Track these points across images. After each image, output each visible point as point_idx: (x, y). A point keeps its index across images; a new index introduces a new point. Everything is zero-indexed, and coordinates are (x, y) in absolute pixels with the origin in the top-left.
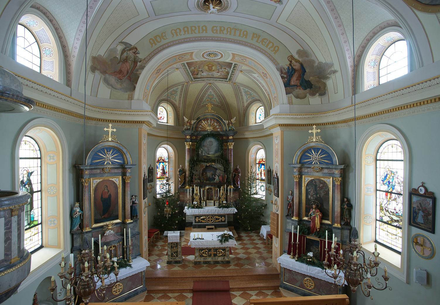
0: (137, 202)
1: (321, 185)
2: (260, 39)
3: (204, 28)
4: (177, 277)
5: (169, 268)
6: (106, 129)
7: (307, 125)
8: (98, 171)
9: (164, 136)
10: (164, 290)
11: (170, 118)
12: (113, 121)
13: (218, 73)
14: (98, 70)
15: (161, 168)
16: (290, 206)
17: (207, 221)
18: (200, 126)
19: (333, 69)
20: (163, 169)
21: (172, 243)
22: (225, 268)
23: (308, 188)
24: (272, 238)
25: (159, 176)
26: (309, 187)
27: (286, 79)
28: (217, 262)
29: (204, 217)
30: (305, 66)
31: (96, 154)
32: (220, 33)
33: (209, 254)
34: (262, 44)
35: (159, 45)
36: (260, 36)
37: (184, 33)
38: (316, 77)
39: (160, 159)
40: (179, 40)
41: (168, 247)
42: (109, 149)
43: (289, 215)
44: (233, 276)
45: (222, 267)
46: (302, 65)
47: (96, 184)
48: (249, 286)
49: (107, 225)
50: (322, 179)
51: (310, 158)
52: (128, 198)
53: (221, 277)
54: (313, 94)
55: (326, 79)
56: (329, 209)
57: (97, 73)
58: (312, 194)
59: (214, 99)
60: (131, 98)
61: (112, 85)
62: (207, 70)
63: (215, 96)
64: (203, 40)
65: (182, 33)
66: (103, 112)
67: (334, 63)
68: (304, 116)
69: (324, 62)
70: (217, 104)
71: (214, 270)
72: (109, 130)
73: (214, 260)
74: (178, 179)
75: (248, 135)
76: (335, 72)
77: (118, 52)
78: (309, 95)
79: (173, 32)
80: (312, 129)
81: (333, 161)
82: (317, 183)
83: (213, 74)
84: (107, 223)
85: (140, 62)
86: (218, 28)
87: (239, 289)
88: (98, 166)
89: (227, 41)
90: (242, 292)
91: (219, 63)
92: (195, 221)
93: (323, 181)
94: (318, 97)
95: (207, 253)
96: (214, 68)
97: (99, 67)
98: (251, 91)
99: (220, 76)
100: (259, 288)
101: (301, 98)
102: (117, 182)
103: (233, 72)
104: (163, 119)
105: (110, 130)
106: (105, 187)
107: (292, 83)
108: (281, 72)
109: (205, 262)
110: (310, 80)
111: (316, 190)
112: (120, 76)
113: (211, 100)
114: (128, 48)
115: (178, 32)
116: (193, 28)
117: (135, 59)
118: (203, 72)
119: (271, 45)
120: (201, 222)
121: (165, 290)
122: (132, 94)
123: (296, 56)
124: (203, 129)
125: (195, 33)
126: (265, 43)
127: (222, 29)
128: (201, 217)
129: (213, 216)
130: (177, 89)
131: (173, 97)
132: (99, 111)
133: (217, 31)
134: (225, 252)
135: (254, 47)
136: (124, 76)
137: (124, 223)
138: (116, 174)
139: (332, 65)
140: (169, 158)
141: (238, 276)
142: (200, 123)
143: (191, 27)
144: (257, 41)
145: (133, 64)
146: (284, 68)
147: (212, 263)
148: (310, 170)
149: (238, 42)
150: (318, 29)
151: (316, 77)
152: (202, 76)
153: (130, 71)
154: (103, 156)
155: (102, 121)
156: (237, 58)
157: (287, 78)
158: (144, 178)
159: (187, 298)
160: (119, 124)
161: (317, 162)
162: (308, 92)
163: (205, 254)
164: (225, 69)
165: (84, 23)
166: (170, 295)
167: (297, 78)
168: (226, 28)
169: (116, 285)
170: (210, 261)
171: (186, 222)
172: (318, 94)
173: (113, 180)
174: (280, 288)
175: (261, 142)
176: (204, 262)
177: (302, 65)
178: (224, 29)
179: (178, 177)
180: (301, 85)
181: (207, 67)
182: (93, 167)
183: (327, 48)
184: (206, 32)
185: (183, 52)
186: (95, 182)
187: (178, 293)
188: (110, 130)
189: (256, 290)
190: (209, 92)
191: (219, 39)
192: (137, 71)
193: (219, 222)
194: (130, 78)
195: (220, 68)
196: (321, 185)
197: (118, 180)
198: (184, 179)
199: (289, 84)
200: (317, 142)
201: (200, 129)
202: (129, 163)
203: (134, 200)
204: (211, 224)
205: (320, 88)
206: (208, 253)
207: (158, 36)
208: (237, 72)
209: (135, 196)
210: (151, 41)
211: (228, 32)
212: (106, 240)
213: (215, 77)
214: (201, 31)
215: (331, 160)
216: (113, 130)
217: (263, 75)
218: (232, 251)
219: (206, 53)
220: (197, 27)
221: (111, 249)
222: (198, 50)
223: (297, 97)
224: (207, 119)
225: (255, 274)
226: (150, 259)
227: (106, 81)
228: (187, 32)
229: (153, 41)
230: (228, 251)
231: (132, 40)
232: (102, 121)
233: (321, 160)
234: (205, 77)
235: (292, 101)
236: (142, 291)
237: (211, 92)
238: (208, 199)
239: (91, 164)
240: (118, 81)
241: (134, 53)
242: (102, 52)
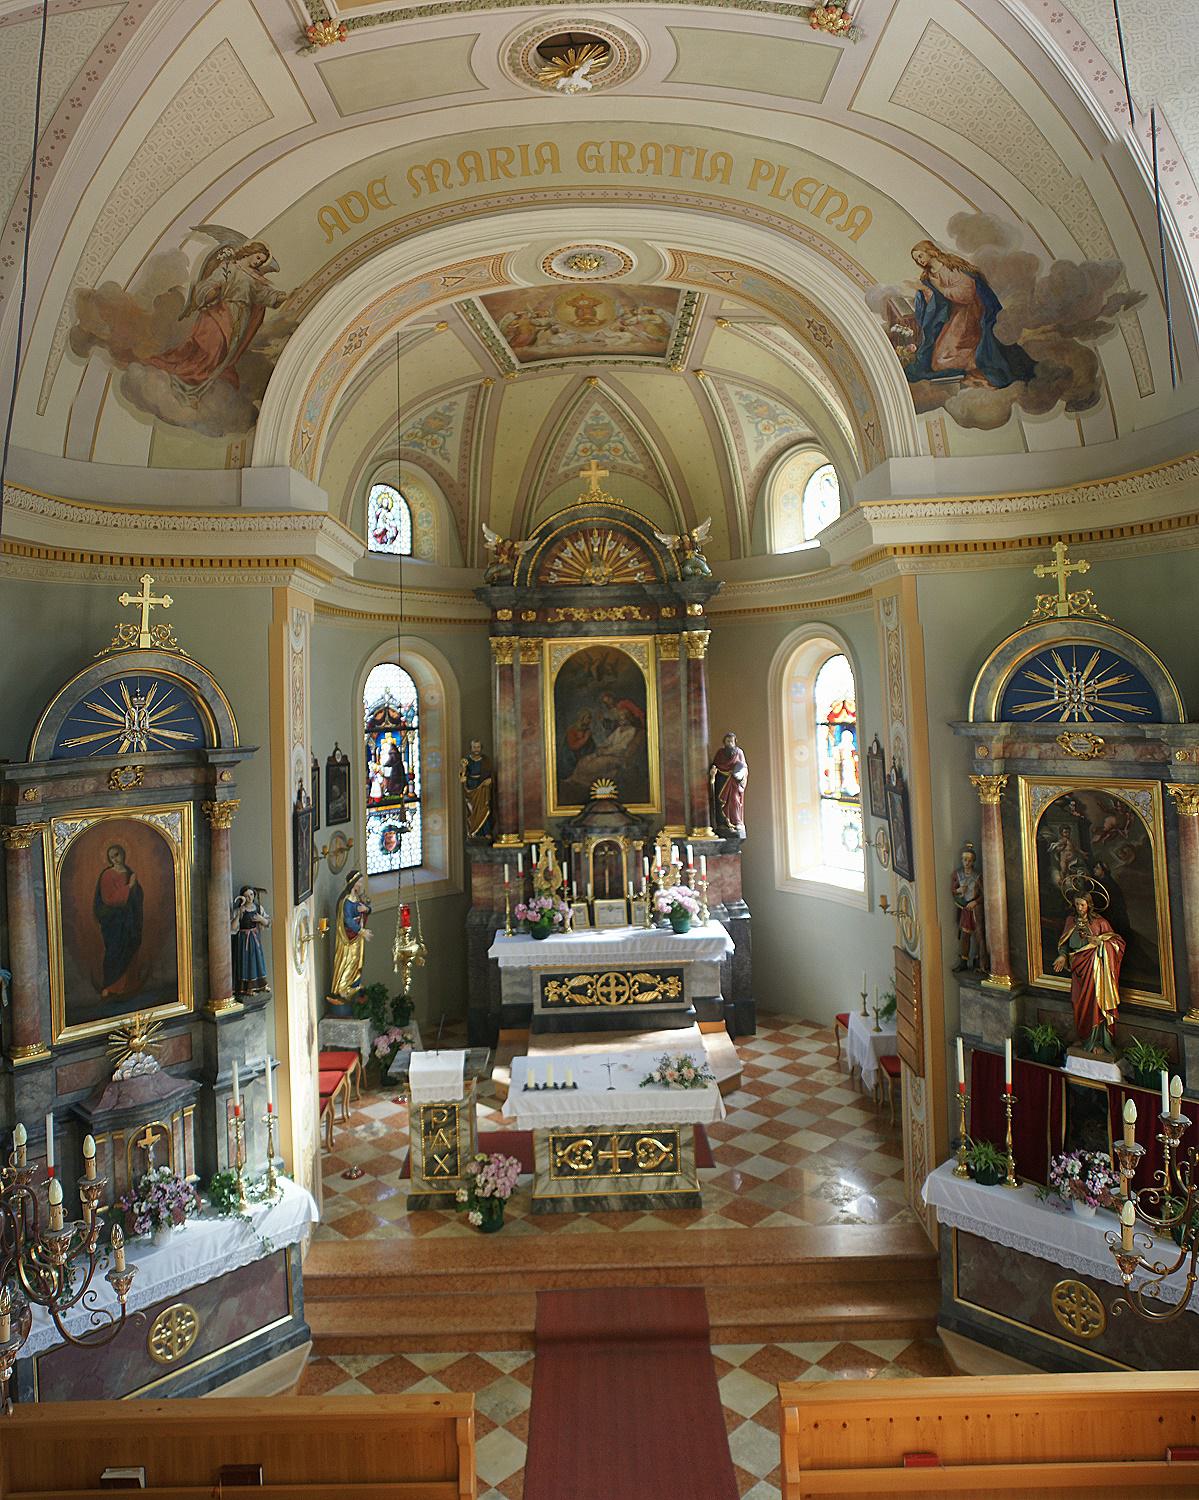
0: (263, 917)
1: (1110, 821)
2: (788, 183)
3: (546, 153)
4: (452, 1271)
5: (418, 1230)
6: (126, 599)
7: (1004, 543)
8: (90, 785)
9: (388, 612)
10: (391, 1337)
11: (425, 534)
12: (132, 560)
13: (622, 330)
14: (102, 343)
15: (385, 757)
16: (968, 918)
17: (598, 1000)
18: (558, 565)
19: (1122, 289)
20: (396, 761)
21: (427, 1109)
22: (677, 1223)
23: (1046, 835)
24: (896, 1075)
25: (376, 792)
26: (1051, 830)
27: (913, 347)
28: (636, 1204)
29: (585, 980)
30: (993, 282)
31: (81, 710)
32: (614, 169)
33: (601, 1163)
34: (799, 204)
35: (357, 232)
36: (783, 171)
37: (462, 179)
38: (1049, 327)
39: (380, 717)
40: (442, 206)
41: (412, 1126)
42: (140, 684)
43: (971, 965)
44: (713, 1267)
45: (666, 1219)
46: (979, 280)
47: (68, 841)
48: (789, 1320)
49: (127, 1033)
50: (1112, 791)
51: (106, 724)
52: (224, 899)
53: (658, 1269)
54: (1040, 405)
55: (1097, 335)
56: (1157, 939)
57: (99, 359)
58: (1067, 863)
59: (613, 445)
60: (240, 461)
61: (157, 408)
62: (572, 323)
63: (617, 429)
64: (566, 200)
65: (456, 176)
66: (116, 526)
67: (694, 1121)
68: (1002, 507)
69: (1078, 260)
70: (629, 463)
71: (625, 1233)
72: (139, 600)
73: (625, 1192)
74: (465, 806)
75: (763, 593)
76: (1132, 300)
77: (189, 269)
78: (1024, 407)
79: (418, 174)
80: (1049, 559)
81: (1157, 702)
82: (1087, 812)
83: (598, 338)
84: (127, 1021)
85: (275, 306)
86: (606, 150)
87: (743, 1334)
88: (90, 760)
89: (644, 201)
90: (759, 1347)
91: (620, 292)
92: (544, 998)
93: (1118, 800)
94: (1062, 415)
95: (589, 1155)
96: (600, 312)
97: (107, 330)
98: (772, 403)
99: (633, 345)
100: (841, 1329)
101: (986, 426)
102: (173, 828)
103: (686, 325)
104: (394, 539)
105: (147, 601)
106: (112, 852)
107: (942, 360)
108: (892, 318)
109: (586, 1200)
110: (1020, 343)
111: (1084, 843)
112: (193, 367)
113: (600, 450)
114: (230, 248)
115: (437, 176)
116: (502, 156)
117: (253, 294)
118: (556, 332)
119: (834, 203)
120: (573, 1004)
121: (398, 1336)
122: (244, 443)
123: (949, 244)
124: (570, 576)
125: (509, 175)
126: (810, 196)
127: (623, 150)
128: (571, 977)
129: (624, 974)
130: (449, 408)
131: (435, 442)
132: (98, 523)
133: (599, 160)
134: (673, 1151)
135: (762, 216)
136: (210, 369)
137: (203, 1015)
138: (168, 796)
139: (1116, 271)
140: (422, 708)
141: (736, 1265)
142: (554, 551)
143: (493, 152)
144: (774, 193)
145: (246, 315)
146: (901, 300)
147: (615, 1205)
148: (1052, 749)
149: (692, 201)
150: (1029, 123)
151: (1049, 327)
152: (555, 350)
153: (232, 347)
154: (114, 716)
155: (112, 563)
156: (691, 268)
157: (915, 339)
158: (296, 807)
159: (496, 1373)
160: (188, 571)
161: (1080, 714)
162: (1015, 395)
163: (584, 1161)
164: (651, 312)
165: (19, 227)
166: (419, 1360)
167: (963, 337)
168: (638, 148)
169: (169, 1317)
170: (606, 1197)
171: (504, 1002)
172: (1061, 403)
173: (157, 820)
174: (939, 1329)
175: (837, 628)
176: (575, 1200)
177: (979, 280)
178: (631, 154)
179: (465, 795)
180: (981, 365)
181: (571, 310)
182: (64, 769)
183: (1088, 198)
184: (556, 169)
185: (503, 245)
186: (64, 831)
187: (455, 1350)
188: (147, 601)
189: (825, 1339)
190: (589, 415)
191: (611, 194)
192: (264, 343)
193: (654, 1001)
194: (233, 378)
195: (628, 309)
196: (1110, 821)
197: (177, 824)
198: (491, 802)
199: (930, 361)
200: (1075, 617)
201: (554, 578)
202: (224, 744)
203: (252, 908)
204: (616, 1010)
205: (1069, 373)
206: (595, 1154)
207: (356, 194)
208: (700, 324)
209: (257, 891)
210: (326, 216)
211: (645, 161)
212: (118, 1103)
213: (609, 349)
214: (533, 165)
215: (1150, 700)
216: (161, 601)
217: (810, 333)
218: (714, 1144)
219: (561, 256)
220: (517, 151)
221: (142, 1143)
222: (522, 245)
223: (968, 422)
224: (587, 534)
225: (800, 1256)
226: (333, 1187)
227: (133, 393)
228: (473, 175)
229: (336, 215)
230: (687, 1145)
231: (247, 217)
232: (112, 563)
233: (1101, 702)
234: (566, 350)
235: (944, 436)
236: (289, 1340)
237: (597, 413)
238: (599, 894)
239: (58, 756)
240: (184, 389)
241: (256, 268)
242: (122, 271)
